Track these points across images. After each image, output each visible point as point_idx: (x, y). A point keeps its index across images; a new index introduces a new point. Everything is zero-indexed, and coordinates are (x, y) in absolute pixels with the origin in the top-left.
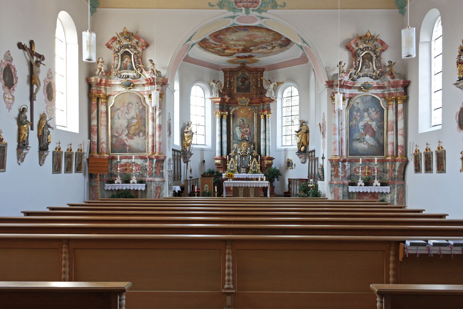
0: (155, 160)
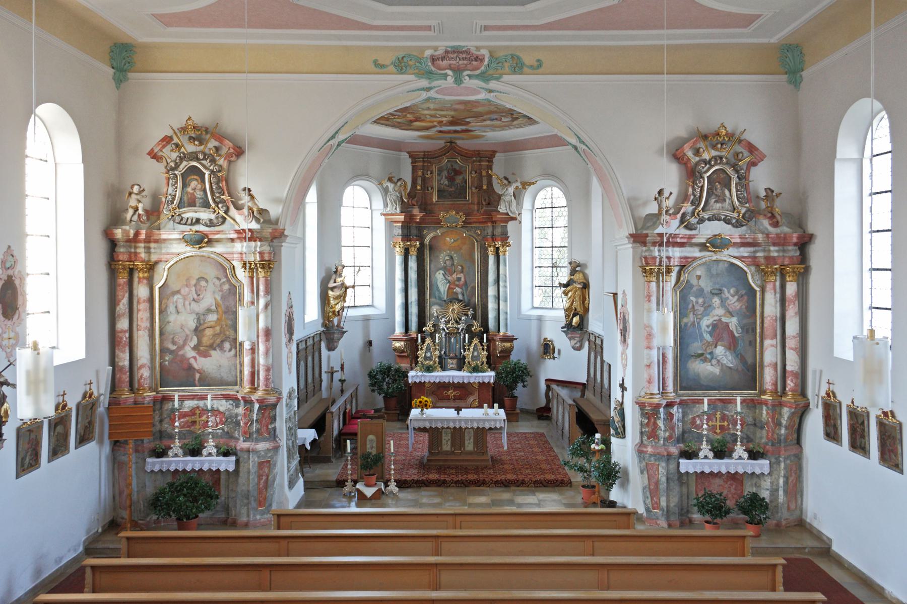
0: (257, 406)
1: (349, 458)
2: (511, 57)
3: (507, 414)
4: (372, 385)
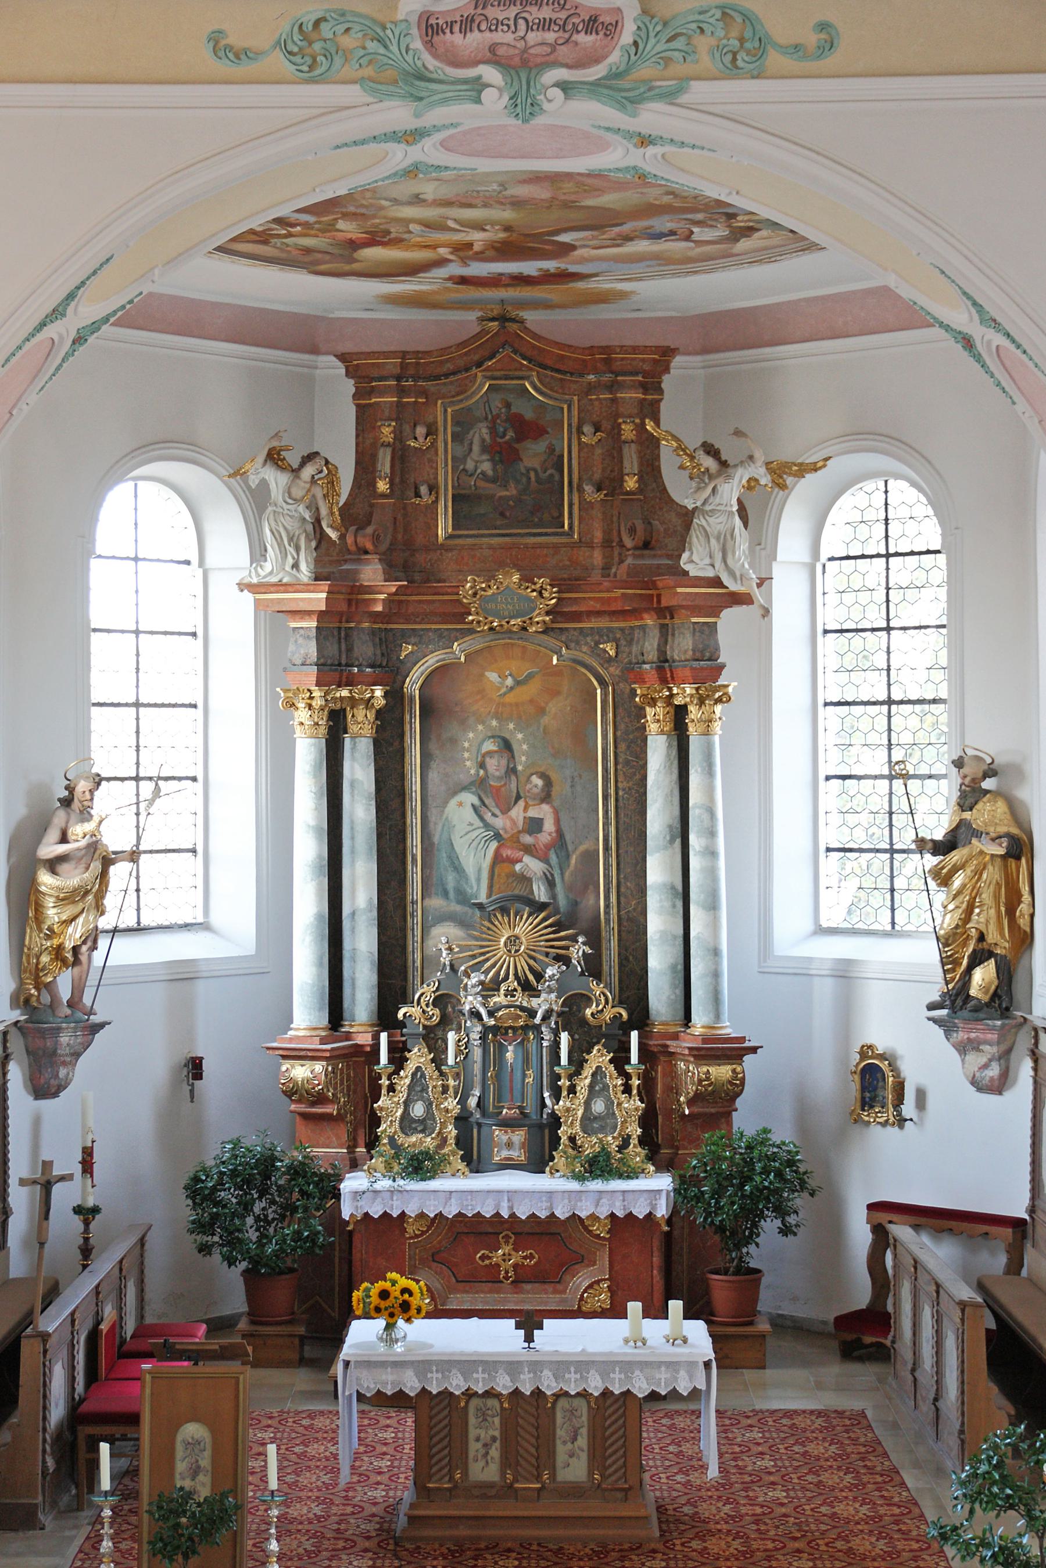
1: (107, 1513)
2: (718, 15)
3: (717, 1339)
4: (201, 1227)
